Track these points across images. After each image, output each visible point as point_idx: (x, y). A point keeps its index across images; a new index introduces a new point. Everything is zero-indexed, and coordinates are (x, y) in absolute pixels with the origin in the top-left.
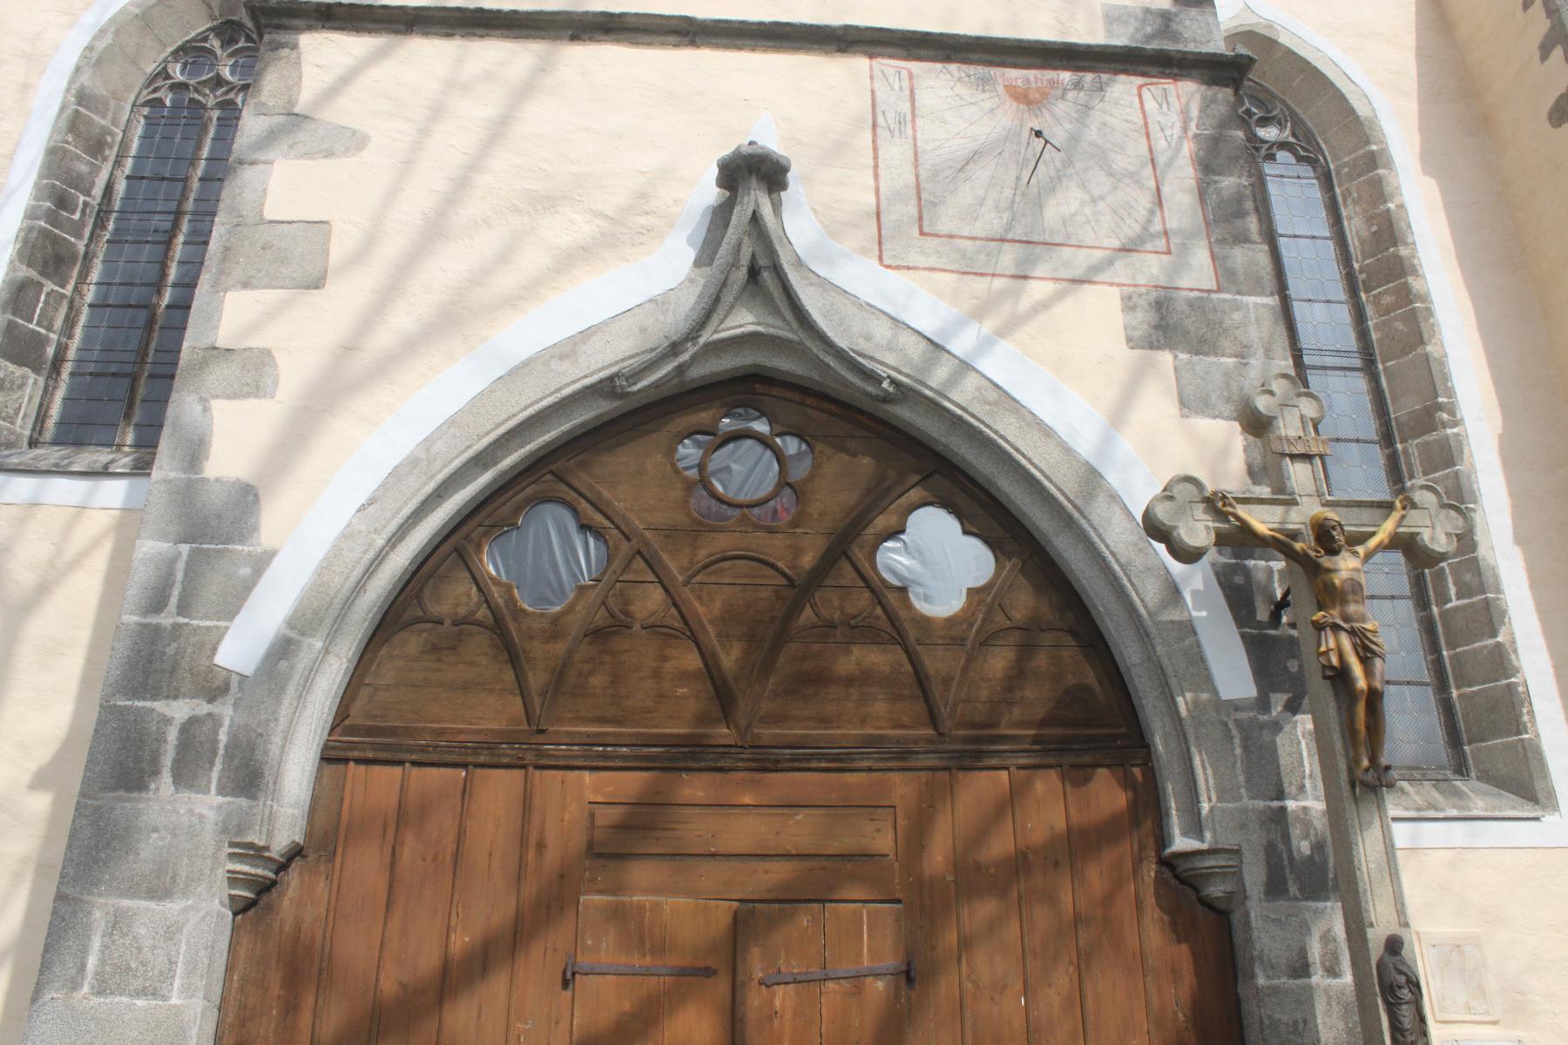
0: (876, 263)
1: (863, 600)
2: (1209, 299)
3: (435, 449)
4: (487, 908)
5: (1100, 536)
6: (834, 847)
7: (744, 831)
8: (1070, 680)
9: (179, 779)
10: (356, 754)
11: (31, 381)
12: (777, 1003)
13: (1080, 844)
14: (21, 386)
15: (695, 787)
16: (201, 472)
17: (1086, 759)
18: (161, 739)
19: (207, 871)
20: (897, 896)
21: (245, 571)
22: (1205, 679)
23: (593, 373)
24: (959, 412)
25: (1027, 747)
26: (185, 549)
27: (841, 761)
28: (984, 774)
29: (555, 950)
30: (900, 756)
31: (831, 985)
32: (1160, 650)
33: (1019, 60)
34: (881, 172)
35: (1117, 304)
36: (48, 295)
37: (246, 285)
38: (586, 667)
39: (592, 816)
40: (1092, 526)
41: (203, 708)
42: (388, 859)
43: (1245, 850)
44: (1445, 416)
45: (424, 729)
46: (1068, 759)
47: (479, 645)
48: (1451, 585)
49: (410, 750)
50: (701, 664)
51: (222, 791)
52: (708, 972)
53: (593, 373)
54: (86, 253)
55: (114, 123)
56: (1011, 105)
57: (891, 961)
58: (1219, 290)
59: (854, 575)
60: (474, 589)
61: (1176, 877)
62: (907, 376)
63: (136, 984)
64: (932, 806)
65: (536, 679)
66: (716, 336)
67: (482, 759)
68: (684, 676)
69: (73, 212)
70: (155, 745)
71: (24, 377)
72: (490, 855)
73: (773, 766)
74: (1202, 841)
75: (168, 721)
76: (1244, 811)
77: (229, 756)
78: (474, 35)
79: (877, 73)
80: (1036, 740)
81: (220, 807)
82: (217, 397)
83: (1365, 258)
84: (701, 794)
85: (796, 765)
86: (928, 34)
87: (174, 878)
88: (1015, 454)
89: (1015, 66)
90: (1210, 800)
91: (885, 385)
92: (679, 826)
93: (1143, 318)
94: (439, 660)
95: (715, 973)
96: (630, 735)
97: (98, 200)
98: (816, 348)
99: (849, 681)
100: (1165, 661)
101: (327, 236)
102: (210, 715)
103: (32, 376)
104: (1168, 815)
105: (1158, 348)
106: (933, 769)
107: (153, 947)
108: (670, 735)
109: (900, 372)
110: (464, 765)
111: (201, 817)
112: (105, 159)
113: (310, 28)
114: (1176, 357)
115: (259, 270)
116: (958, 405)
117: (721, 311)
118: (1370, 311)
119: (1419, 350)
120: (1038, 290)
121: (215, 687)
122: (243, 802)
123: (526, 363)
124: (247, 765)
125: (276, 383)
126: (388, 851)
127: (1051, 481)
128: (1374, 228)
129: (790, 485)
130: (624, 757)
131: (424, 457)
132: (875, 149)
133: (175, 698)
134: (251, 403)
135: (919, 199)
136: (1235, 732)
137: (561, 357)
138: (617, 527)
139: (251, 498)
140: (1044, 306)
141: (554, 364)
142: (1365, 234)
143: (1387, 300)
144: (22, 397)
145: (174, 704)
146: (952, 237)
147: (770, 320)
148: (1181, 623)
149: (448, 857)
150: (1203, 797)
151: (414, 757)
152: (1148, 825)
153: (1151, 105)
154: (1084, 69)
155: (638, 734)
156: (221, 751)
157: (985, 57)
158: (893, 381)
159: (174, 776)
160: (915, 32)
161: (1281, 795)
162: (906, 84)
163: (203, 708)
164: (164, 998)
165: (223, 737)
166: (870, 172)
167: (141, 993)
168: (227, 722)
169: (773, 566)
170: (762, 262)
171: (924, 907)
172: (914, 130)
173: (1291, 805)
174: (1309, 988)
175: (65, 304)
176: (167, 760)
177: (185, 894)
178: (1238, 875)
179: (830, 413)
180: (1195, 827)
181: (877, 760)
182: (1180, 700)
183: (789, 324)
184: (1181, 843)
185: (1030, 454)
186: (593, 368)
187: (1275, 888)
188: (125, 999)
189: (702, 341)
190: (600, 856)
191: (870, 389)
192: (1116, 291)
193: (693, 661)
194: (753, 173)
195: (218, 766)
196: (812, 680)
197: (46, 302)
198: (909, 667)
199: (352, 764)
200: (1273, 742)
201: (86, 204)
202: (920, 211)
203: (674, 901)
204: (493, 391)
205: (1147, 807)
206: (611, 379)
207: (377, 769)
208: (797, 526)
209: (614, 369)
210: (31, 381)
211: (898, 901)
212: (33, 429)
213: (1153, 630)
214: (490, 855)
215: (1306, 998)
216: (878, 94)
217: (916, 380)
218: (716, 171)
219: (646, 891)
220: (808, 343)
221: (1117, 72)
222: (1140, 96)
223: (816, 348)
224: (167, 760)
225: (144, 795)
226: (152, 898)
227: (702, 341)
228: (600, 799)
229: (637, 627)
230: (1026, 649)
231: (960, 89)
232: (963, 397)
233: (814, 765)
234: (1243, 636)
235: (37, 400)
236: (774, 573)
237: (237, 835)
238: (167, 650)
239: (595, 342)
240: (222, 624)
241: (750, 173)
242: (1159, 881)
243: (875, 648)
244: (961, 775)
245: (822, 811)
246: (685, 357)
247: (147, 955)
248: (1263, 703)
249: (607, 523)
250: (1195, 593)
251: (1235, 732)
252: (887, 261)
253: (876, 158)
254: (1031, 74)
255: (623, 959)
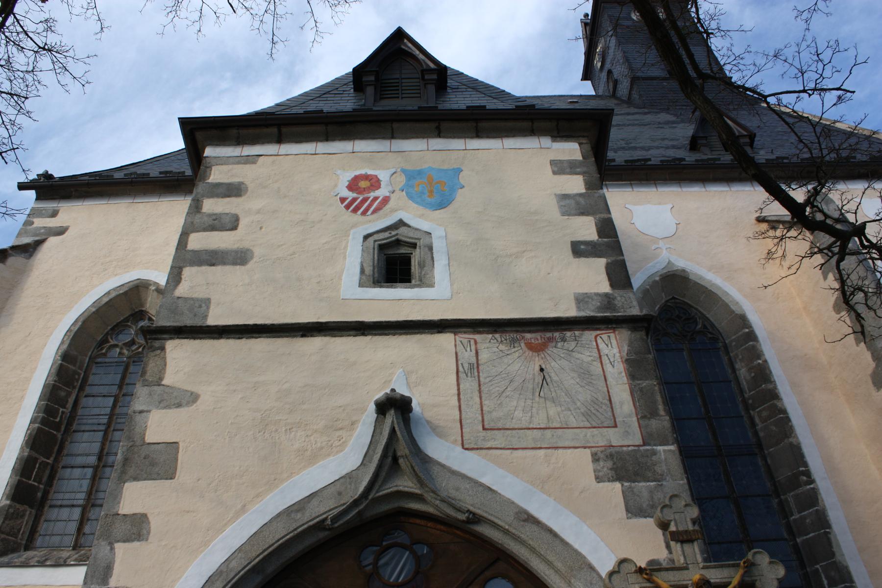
0: (459, 448)
2: (639, 450)
3: (231, 566)
11: (28, 513)
14: (23, 516)
34: (461, 397)
35: (589, 458)
36: (40, 464)
37: (136, 479)
44: (805, 478)
48: (824, 579)
54: (62, 439)
55: (80, 368)
58: (644, 444)
66: (378, 495)
69: (56, 418)
71: (25, 511)
78: (253, 337)
79: (458, 342)
82: (118, 541)
83: (750, 391)
89: (529, 332)
93: (606, 466)
97: (70, 410)
101: (178, 449)
103: (28, 511)
112: (74, 387)
113: (171, 339)
114: (622, 485)
115: (142, 470)
117: (376, 487)
118: (757, 420)
119: (786, 441)
125: (149, 533)
128: (753, 374)
132: (458, 385)
134: (136, 544)
135: (482, 410)
137: (298, 511)
142: (748, 378)
143: (765, 414)
144: (22, 522)
153: (602, 346)
154: (566, 330)
160: (476, 320)
162: (473, 347)
166: (456, 398)
172: (478, 372)
175: (49, 467)
189: (370, 497)
192: (588, 451)
194: (394, 407)
197: (39, 468)
201: (63, 412)
202: (483, 417)
210: (28, 513)
212: (27, 540)
214: (511, 381)
216: (459, 354)
218: (374, 407)
221: (583, 330)
222: (596, 341)
227: (370, 497)
231: (502, 347)
235: (31, 523)
239: (315, 502)
246: (361, 507)
252: (466, 446)
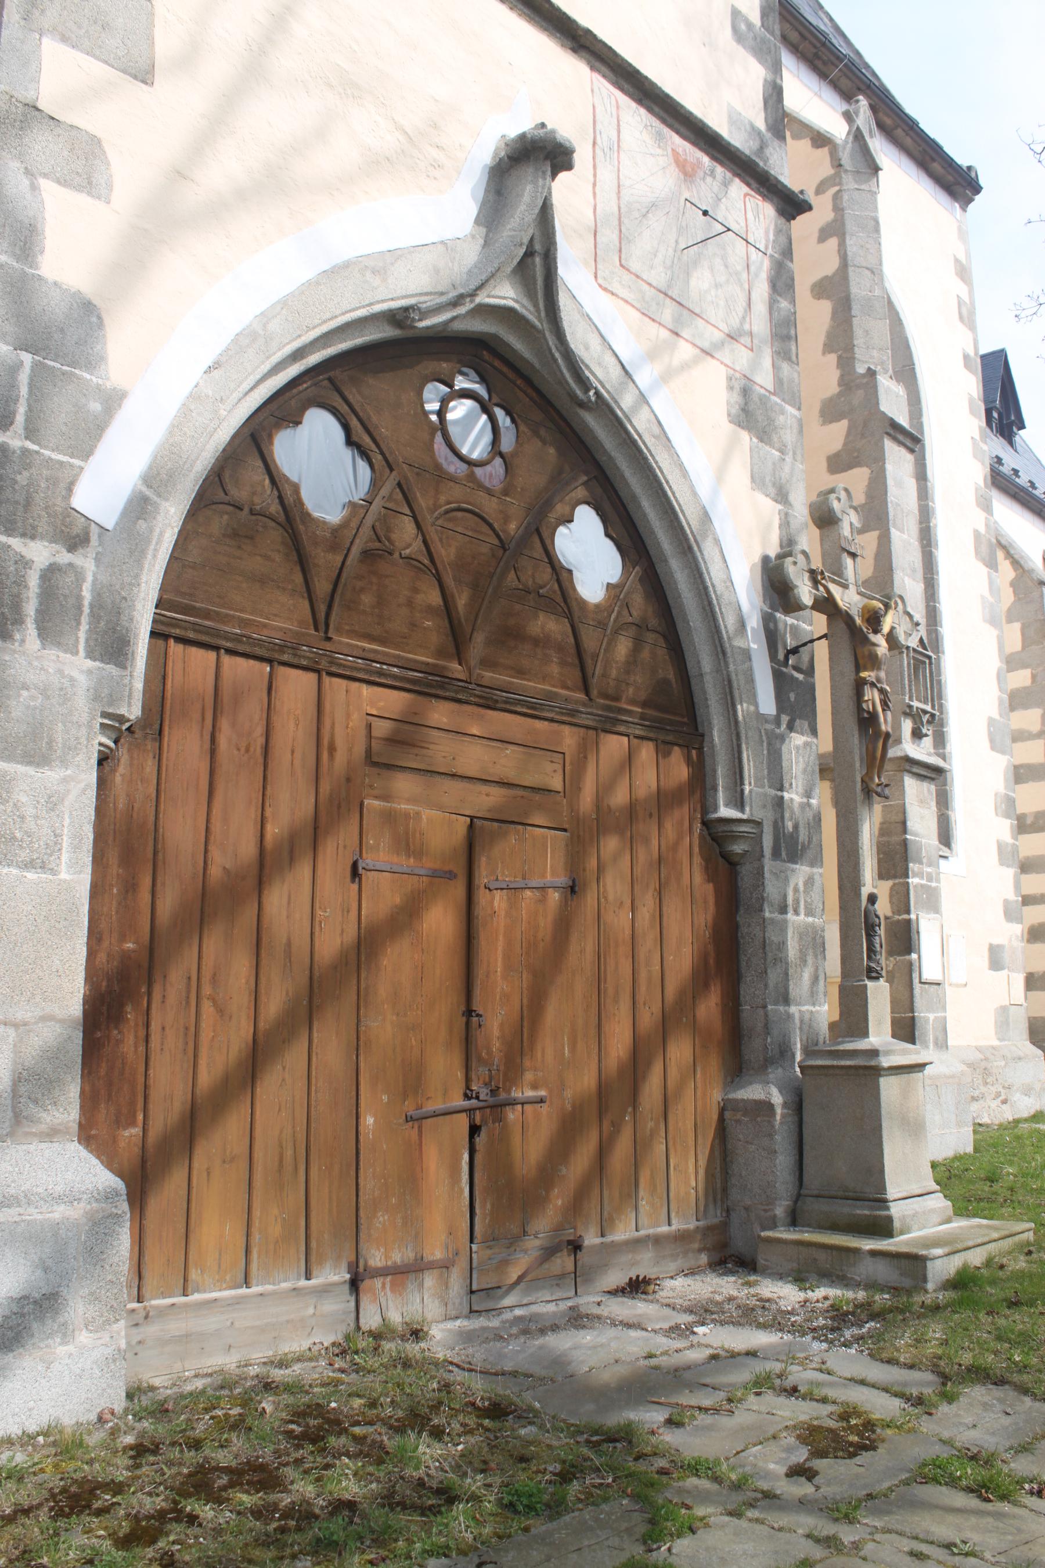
1: (545, 574)
4: (291, 805)
5: (707, 569)
6: (529, 780)
7: (473, 757)
8: (661, 674)
9: (44, 633)
10: (178, 631)
12: (496, 904)
13: (664, 801)
15: (440, 713)
16: (37, 268)
17: (670, 738)
18: (21, 583)
19: (83, 741)
20: (566, 826)
21: (96, 407)
22: (753, 699)
23: (398, 298)
24: (636, 437)
25: (636, 720)
26: (27, 358)
27: (535, 709)
28: (615, 737)
29: (345, 847)
30: (569, 717)
31: (528, 893)
32: (732, 667)
33: (682, 129)
38: (359, 584)
39: (369, 726)
40: (703, 559)
41: (64, 557)
42: (207, 745)
43: (765, 823)
45: (233, 617)
46: (662, 737)
47: (273, 537)
49: (227, 637)
50: (442, 603)
51: (90, 655)
52: (451, 876)
53: (398, 298)
56: (674, 171)
57: (562, 880)
58: (774, 394)
59: (541, 550)
60: (267, 481)
61: (710, 834)
62: (608, 392)
63: (24, 855)
64: (585, 757)
65: (322, 587)
67: (285, 657)
68: (430, 610)
70: (15, 590)
72: (293, 752)
73: (489, 705)
74: (743, 811)
75: (25, 563)
76: (765, 795)
77: (94, 616)
80: (643, 717)
81: (90, 672)
82: (45, 176)
84: (445, 720)
85: (508, 707)
86: (638, 72)
87: (50, 743)
88: (665, 485)
90: (750, 783)
91: (592, 393)
92: (431, 746)
94: (239, 547)
95: (455, 876)
96: (423, 663)
98: (551, 341)
99: (536, 642)
100: (734, 677)
102: (70, 565)
104: (715, 789)
105: (743, 428)
106: (587, 727)
107: (36, 817)
108: (416, 661)
109: (603, 387)
110: (270, 661)
111: (72, 680)
116: (636, 431)
120: (685, 351)
121: (75, 534)
122: (111, 669)
123: (347, 265)
124: (114, 631)
126: (207, 737)
127: (684, 515)
129: (501, 455)
130: (395, 677)
131: (262, 332)
133: (33, 538)
136: (764, 738)
138: (382, 453)
139: (94, 319)
140: (685, 366)
141: (368, 275)
145: (32, 544)
146: (638, 277)
147: (525, 301)
148: (744, 650)
149: (259, 751)
150: (746, 782)
151: (228, 645)
152: (697, 796)
155: (399, 656)
156: (86, 610)
157: (662, 113)
158: (597, 393)
159: (38, 629)
161: (781, 789)
163: (64, 557)
164: (54, 872)
165: (87, 594)
167: (29, 865)
168: (90, 578)
169: (490, 525)
170: (538, 247)
171: (581, 836)
173: (786, 795)
174: (786, 921)
176: (30, 608)
177: (64, 763)
178: (758, 839)
179: (531, 399)
180: (739, 801)
181: (557, 713)
182: (739, 707)
183: (538, 310)
184: (725, 812)
185: (674, 488)
186: (399, 293)
187: (776, 854)
188: (14, 871)
190: (376, 764)
191: (579, 392)
193: (434, 598)
195: (84, 627)
196: (510, 636)
198: (572, 640)
199: (172, 642)
200: (780, 749)
203: (427, 814)
204: (318, 283)
205: (700, 783)
206: (406, 309)
207: (194, 651)
208: (506, 495)
209: (412, 301)
211: (565, 830)
213: (729, 651)
214: (293, 752)
215: (783, 926)
217: (613, 398)
219: (408, 801)
220: (547, 334)
223: (551, 341)
224: (30, 608)
225: (8, 645)
226: (29, 763)
228: (375, 712)
229: (396, 555)
230: (638, 643)
232: (640, 424)
233: (519, 709)
234: (772, 667)
236: (491, 532)
237: (111, 704)
238: (19, 478)
240: (76, 462)
241: (546, 158)
242: (701, 837)
243: (553, 617)
244: (602, 735)
245: (521, 749)
247: (30, 824)
248: (777, 721)
249: (373, 447)
250: (753, 628)
251: (764, 738)
252: (600, 281)
253: (595, 175)
254: (687, 146)
255: (395, 859)
